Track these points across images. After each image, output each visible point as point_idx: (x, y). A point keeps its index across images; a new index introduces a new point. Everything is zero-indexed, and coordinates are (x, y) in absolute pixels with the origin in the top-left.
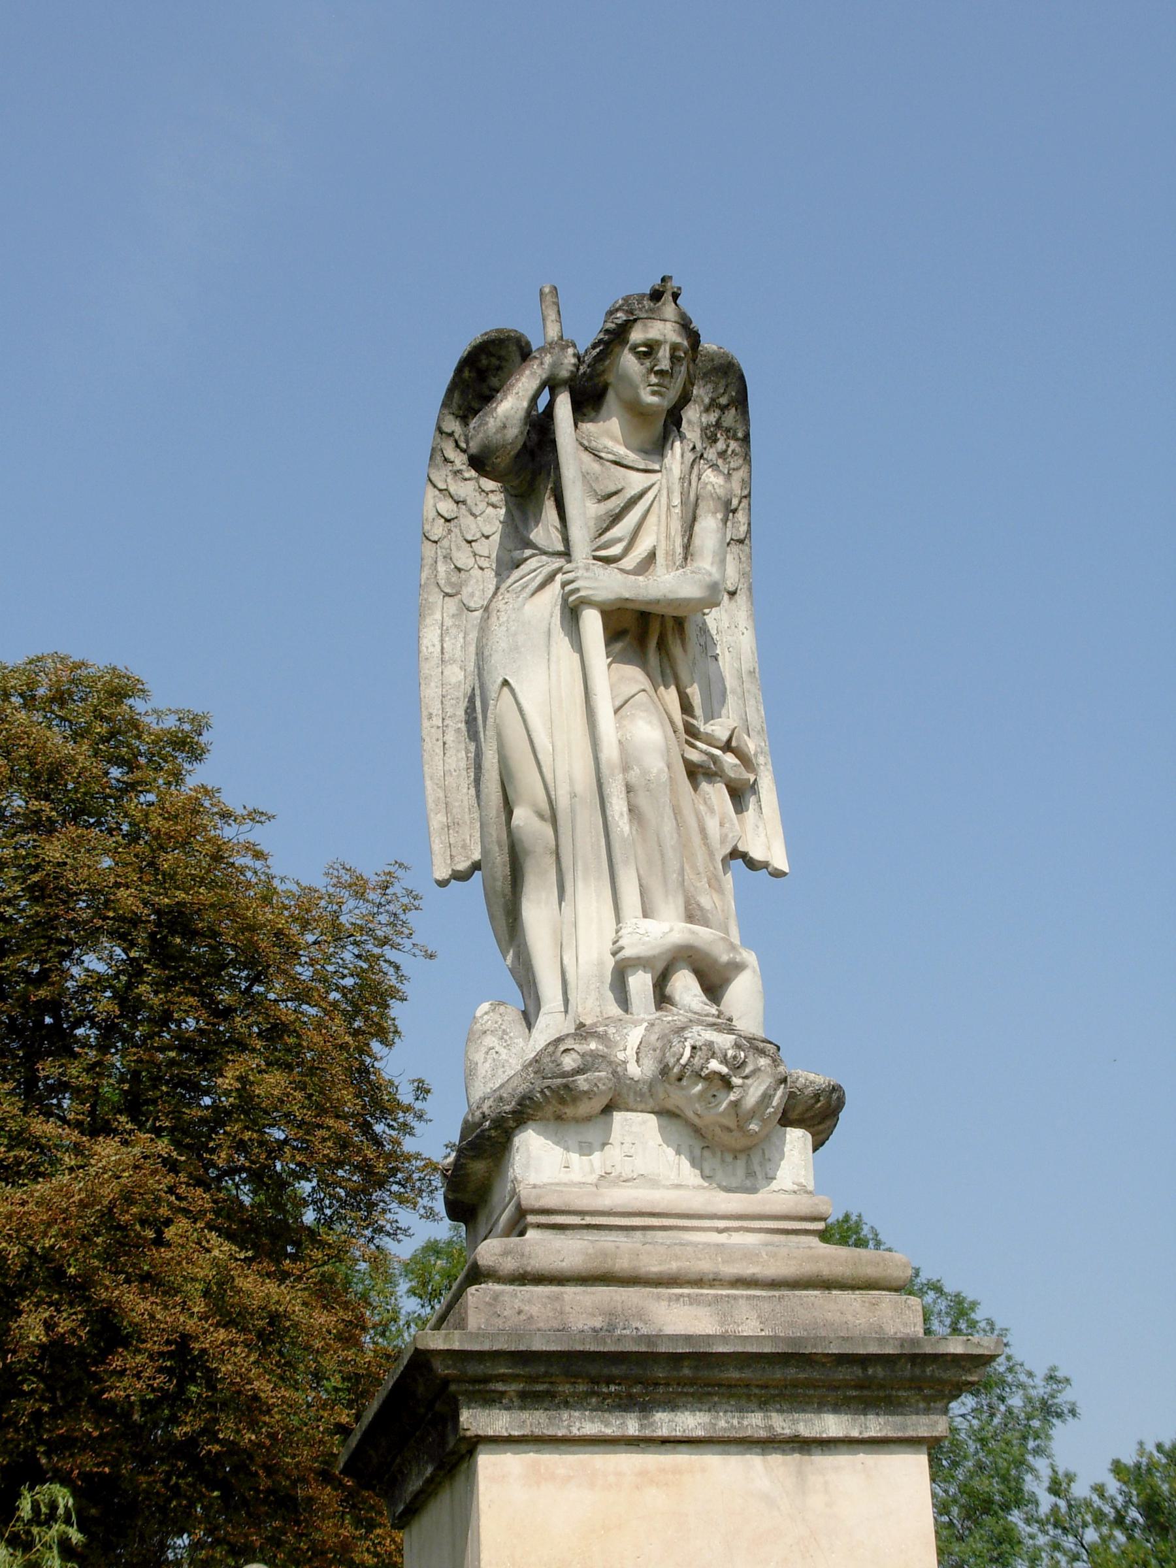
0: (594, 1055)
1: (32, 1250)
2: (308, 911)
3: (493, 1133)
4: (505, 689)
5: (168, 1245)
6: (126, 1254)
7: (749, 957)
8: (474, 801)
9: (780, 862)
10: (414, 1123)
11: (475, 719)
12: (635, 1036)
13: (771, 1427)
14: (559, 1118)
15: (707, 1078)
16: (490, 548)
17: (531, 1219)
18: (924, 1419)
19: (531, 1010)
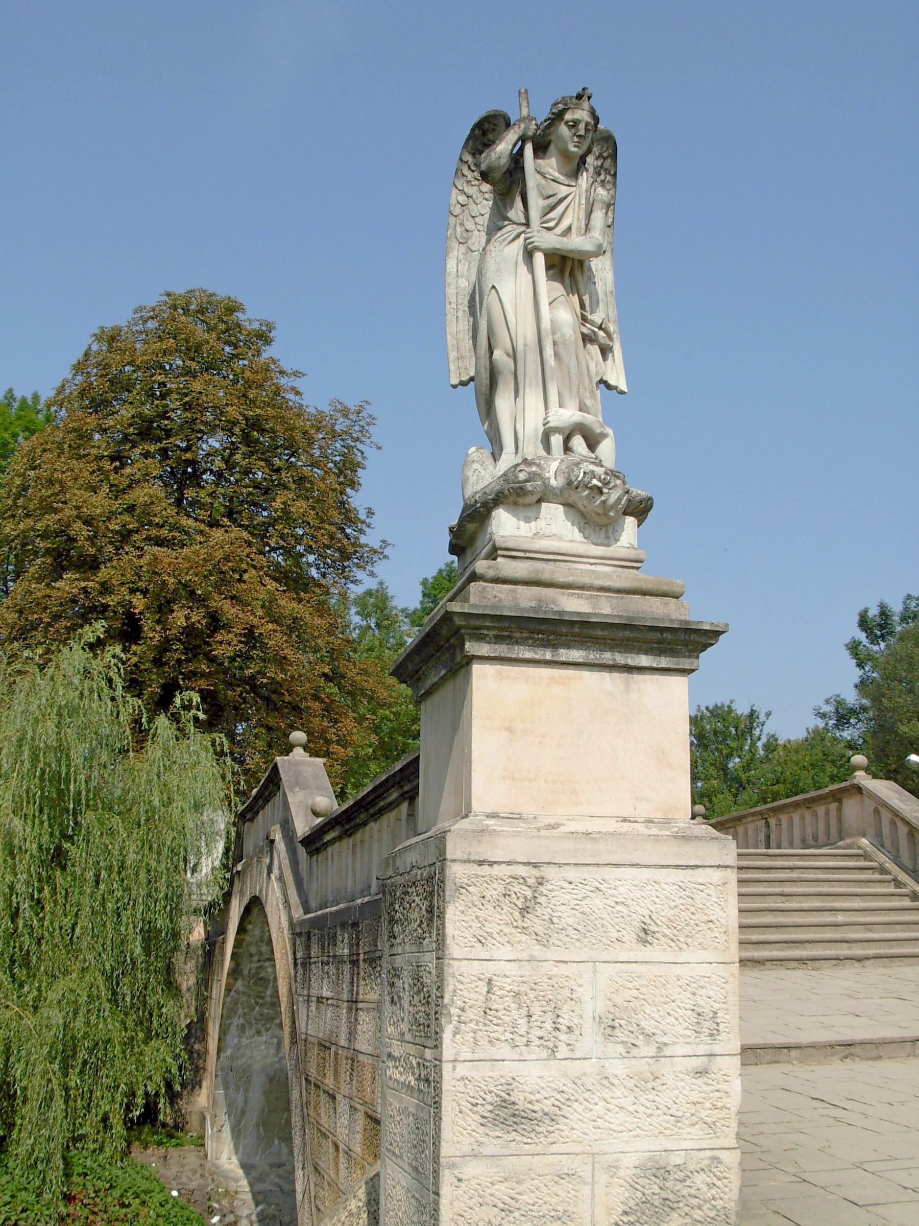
0: (534, 473)
1: (180, 582)
2: (320, 422)
3: (481, 509)
4: (493, 290)
5: (244, 582)
6: (226, 585)
7: (609, 431)
8: (472, 347)
9: (623, 387)
10: (366, 529)
11: (475, 305)
12: (554, 466)
13: (615, 660)
14: (515, 504)
15: (590, 488)
16: (484, 221)
17: (500, 552)
18: (687, 660)
19: (496, 452)
